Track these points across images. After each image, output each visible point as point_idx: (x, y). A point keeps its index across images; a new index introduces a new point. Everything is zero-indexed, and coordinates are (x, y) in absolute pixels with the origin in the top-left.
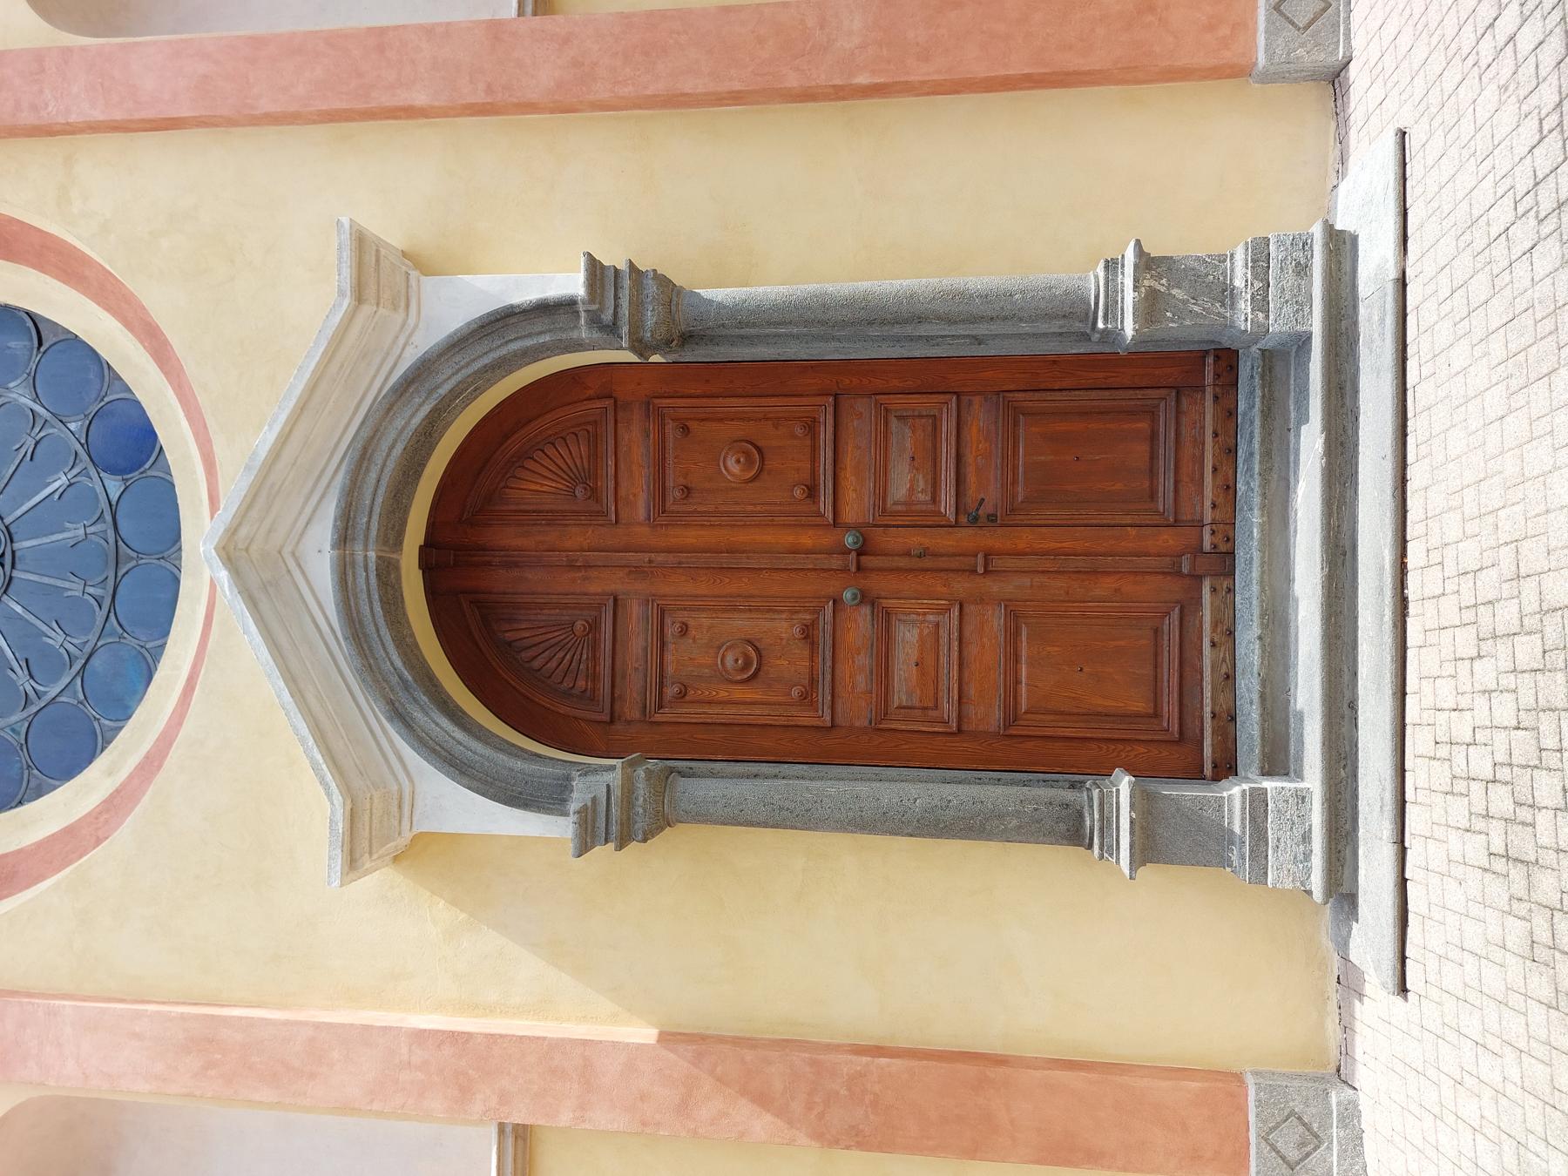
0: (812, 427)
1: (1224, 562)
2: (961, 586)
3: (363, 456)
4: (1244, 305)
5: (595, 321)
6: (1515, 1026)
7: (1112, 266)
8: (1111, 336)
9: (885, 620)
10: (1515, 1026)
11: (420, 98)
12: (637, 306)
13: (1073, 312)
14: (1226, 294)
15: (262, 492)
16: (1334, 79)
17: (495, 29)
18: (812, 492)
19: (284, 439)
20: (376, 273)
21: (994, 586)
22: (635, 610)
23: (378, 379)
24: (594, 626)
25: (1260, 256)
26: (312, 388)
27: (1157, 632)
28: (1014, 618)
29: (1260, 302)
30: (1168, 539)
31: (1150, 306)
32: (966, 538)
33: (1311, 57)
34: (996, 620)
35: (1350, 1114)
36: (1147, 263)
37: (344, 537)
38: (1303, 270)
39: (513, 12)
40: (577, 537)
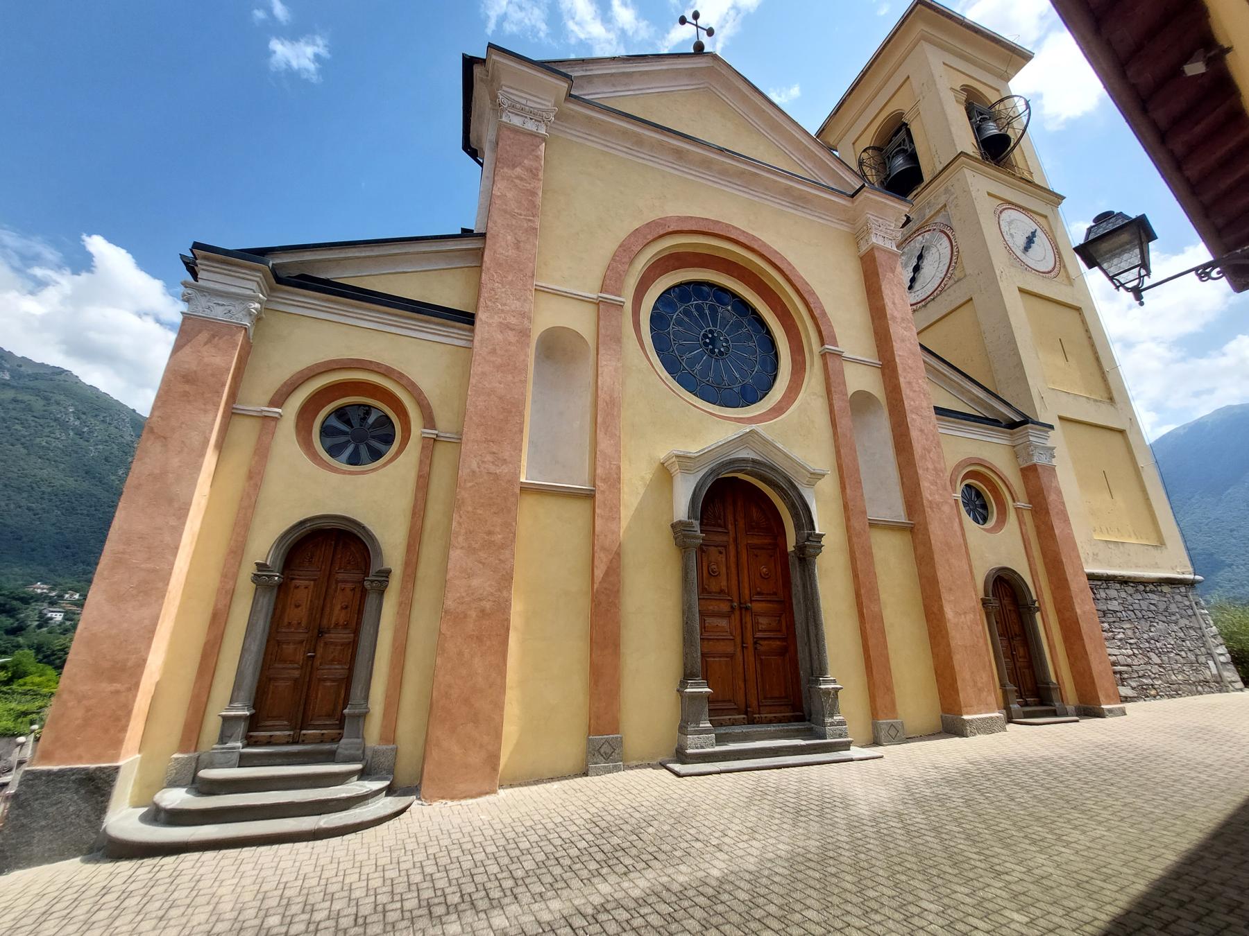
0: (775, 594)
1: (751, 722)
2: (738, 640)
3: (773, 468)
4: (830, 720)
5: (810, 535)
6: (295, 909)
7: (834, 681)
8: (817, 682)
9: (727, 616)
10: (295, 909)
11: (848, 491)
12: (814, 547)
13: (822, 671)
14: (832, 716)
15: (765, 441)
16: (876, 742)
17: (865, 512)
18: (759, 594)
19: (779, 450)
20: (818, 476)
21: (739, 649)
22: (725, 538)
23: (791, 473)
24: (720, 526)
25: (841, 723)
26: (791, 458)
27: (730, 701)
28: (732, 656)
29: (832, 724)
30: (755, 703)
31: (827, 692)
32: (750, 641)
33: (883, 734)
34: (730, 649)
35: (617, 769)
36: (837, 690)
37: (754, 461)
38: (840, 736)
39: (1088, 570)
40: (741, 523)
